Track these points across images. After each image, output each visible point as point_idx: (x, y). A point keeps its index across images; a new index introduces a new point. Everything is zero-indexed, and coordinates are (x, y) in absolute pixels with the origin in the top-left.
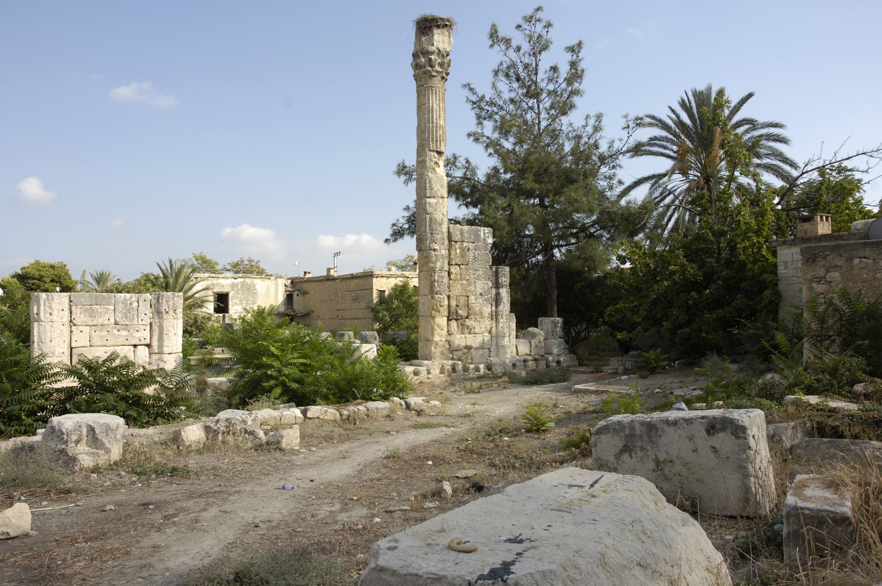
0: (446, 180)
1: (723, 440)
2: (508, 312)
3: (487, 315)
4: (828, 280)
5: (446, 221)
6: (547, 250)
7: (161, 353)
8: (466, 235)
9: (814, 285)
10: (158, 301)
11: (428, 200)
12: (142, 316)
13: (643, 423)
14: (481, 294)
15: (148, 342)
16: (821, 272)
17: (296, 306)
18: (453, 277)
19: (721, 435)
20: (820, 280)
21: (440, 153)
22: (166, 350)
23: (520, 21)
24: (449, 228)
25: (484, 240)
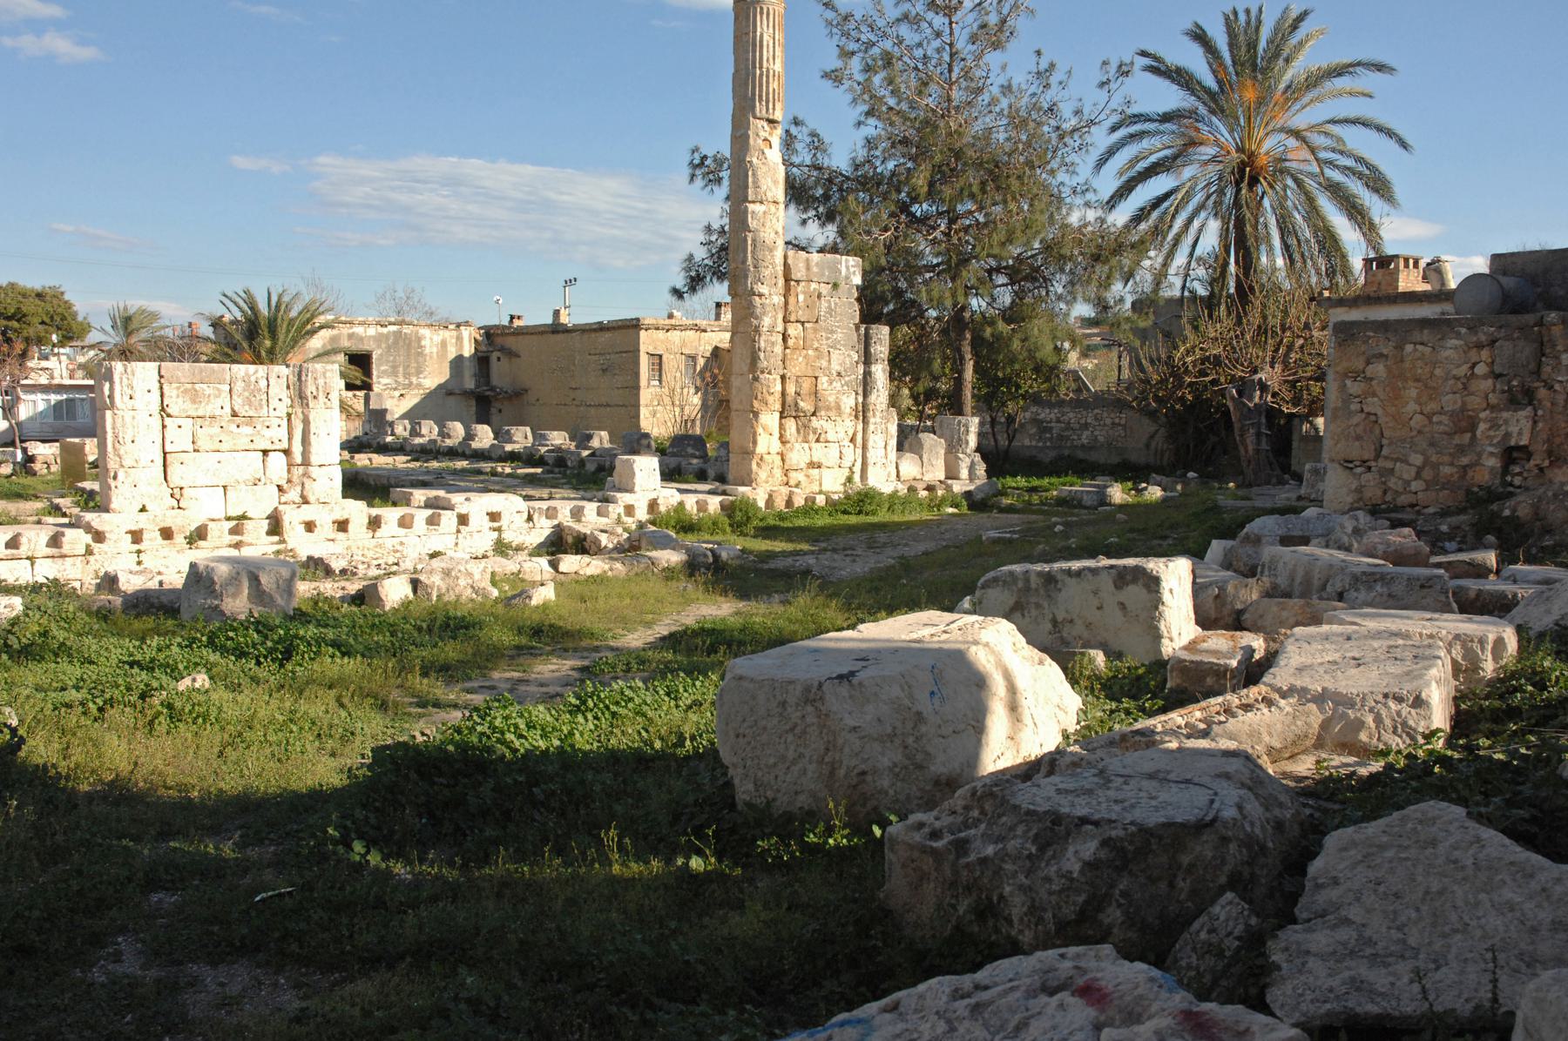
0: (781, 172)
1: (1134, 593)
2: (884, 407)
3: (848, 410)
4: (1368, 374)
5: (780, 243)
7: (306, 462)
8: (815, 269)
9: (1348, 382)
10: (300, 379)
11: (751, 207)
12: (274, 403)
13: (1040, 574)
14: (839, 374)
15: (285, 445)
16: (1359, 364)
17: (496, 380)
18: (791, 342)
20: (1356, 375)
21: (771, 122)
22: (314, 459)
24: (785, 257)
25: (847, 278)
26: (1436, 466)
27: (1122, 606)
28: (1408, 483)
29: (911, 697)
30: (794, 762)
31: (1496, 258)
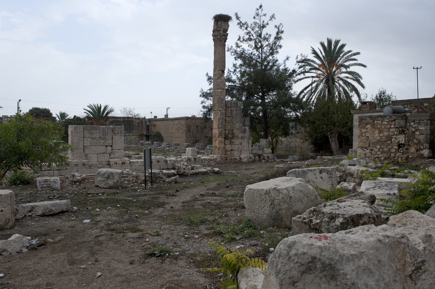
6: (241, 100)
9: (362, 130)
15: (111, 145)
18: (227, 121)
19: (323, 173)
23: (268, 34)
26: (383, 148)
27: (322, 178)
28: (377, 152)
29: (289, 193)
30: (263, 207)
31: (75, 116)
